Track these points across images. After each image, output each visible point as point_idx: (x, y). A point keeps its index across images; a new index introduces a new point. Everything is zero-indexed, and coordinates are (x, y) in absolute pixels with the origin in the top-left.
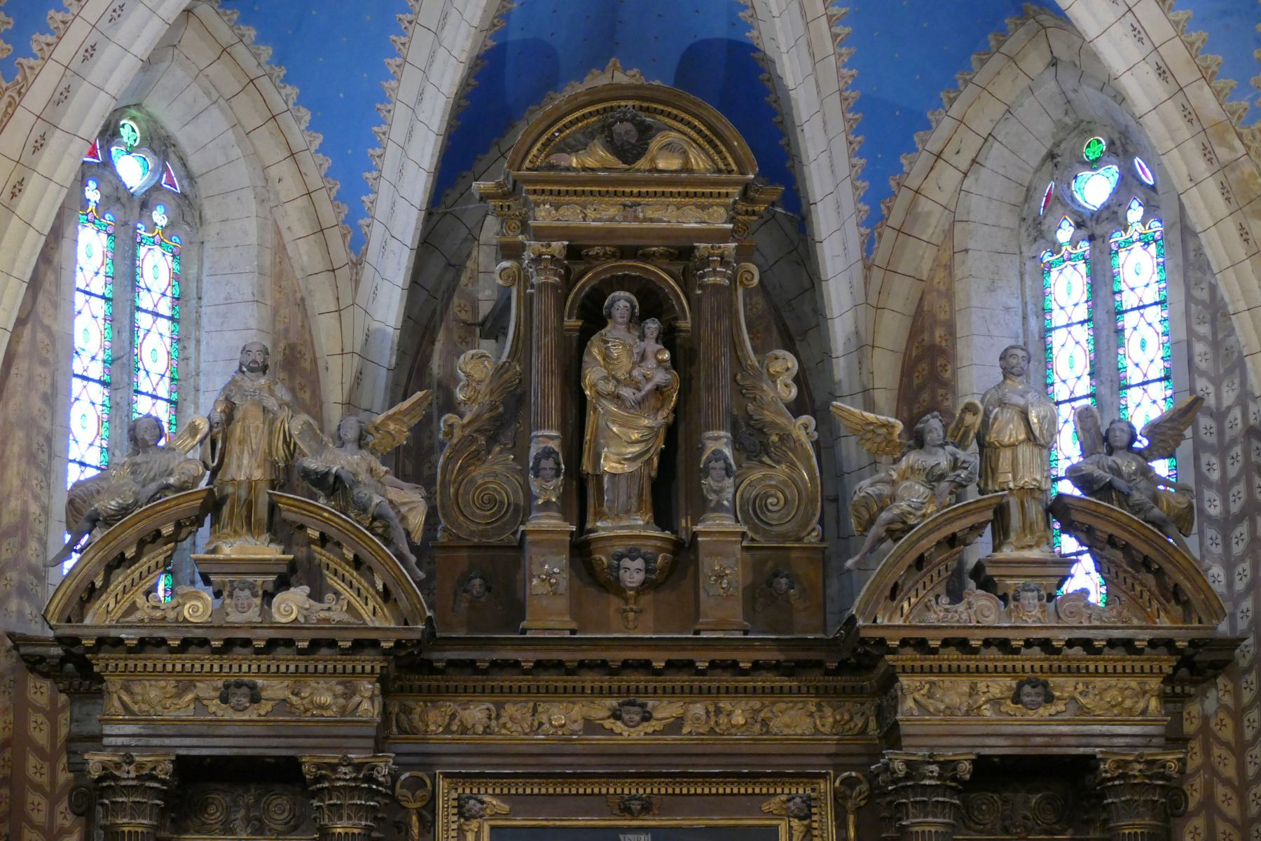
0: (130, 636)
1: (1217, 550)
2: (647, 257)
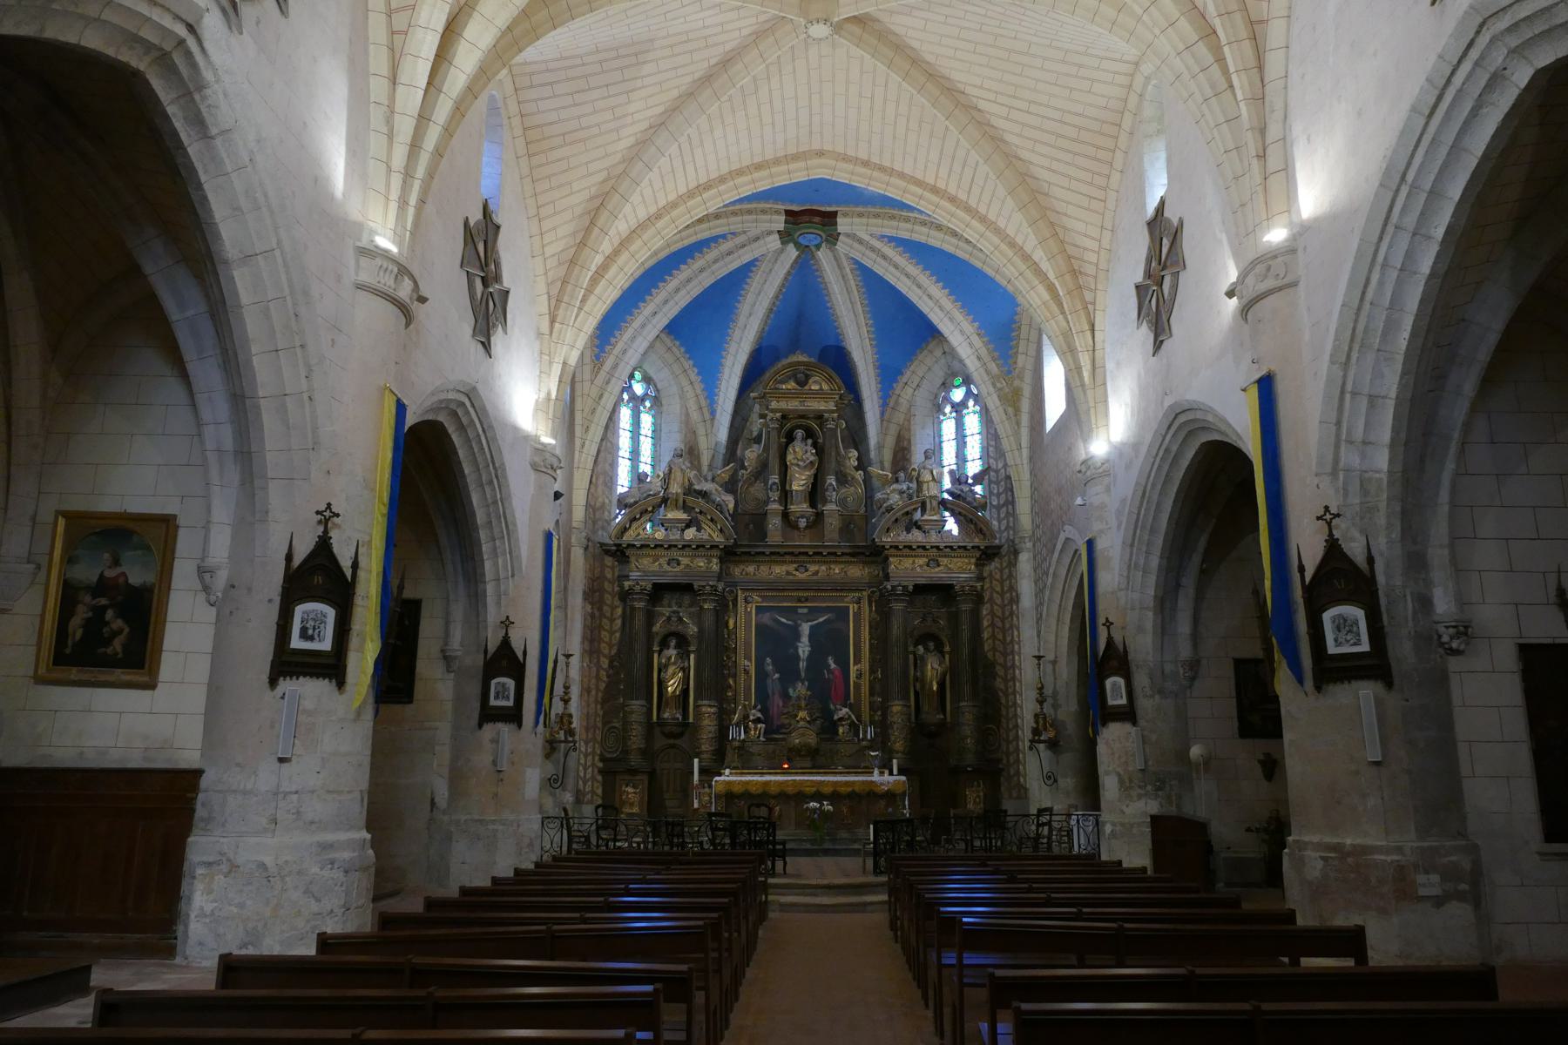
0: (638, 544)
1: (996, 516)
2: (808, 419)
